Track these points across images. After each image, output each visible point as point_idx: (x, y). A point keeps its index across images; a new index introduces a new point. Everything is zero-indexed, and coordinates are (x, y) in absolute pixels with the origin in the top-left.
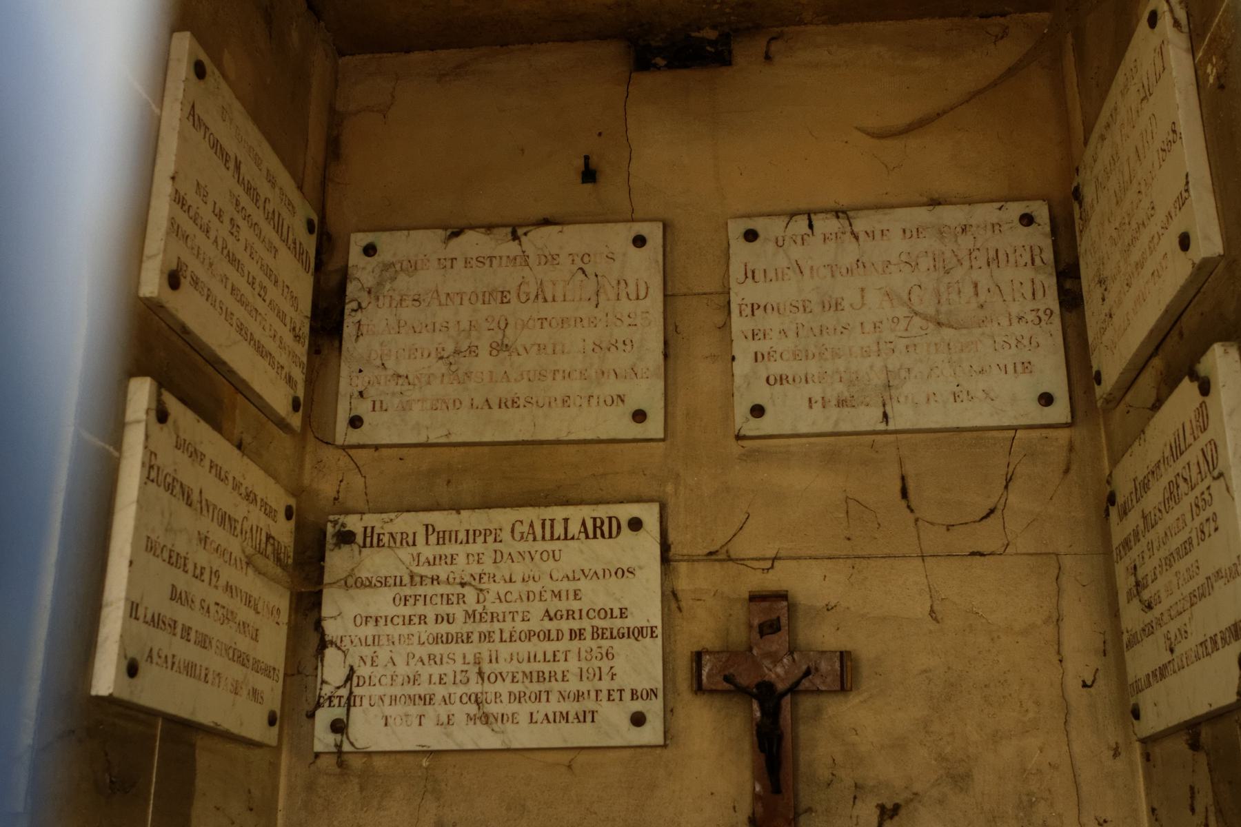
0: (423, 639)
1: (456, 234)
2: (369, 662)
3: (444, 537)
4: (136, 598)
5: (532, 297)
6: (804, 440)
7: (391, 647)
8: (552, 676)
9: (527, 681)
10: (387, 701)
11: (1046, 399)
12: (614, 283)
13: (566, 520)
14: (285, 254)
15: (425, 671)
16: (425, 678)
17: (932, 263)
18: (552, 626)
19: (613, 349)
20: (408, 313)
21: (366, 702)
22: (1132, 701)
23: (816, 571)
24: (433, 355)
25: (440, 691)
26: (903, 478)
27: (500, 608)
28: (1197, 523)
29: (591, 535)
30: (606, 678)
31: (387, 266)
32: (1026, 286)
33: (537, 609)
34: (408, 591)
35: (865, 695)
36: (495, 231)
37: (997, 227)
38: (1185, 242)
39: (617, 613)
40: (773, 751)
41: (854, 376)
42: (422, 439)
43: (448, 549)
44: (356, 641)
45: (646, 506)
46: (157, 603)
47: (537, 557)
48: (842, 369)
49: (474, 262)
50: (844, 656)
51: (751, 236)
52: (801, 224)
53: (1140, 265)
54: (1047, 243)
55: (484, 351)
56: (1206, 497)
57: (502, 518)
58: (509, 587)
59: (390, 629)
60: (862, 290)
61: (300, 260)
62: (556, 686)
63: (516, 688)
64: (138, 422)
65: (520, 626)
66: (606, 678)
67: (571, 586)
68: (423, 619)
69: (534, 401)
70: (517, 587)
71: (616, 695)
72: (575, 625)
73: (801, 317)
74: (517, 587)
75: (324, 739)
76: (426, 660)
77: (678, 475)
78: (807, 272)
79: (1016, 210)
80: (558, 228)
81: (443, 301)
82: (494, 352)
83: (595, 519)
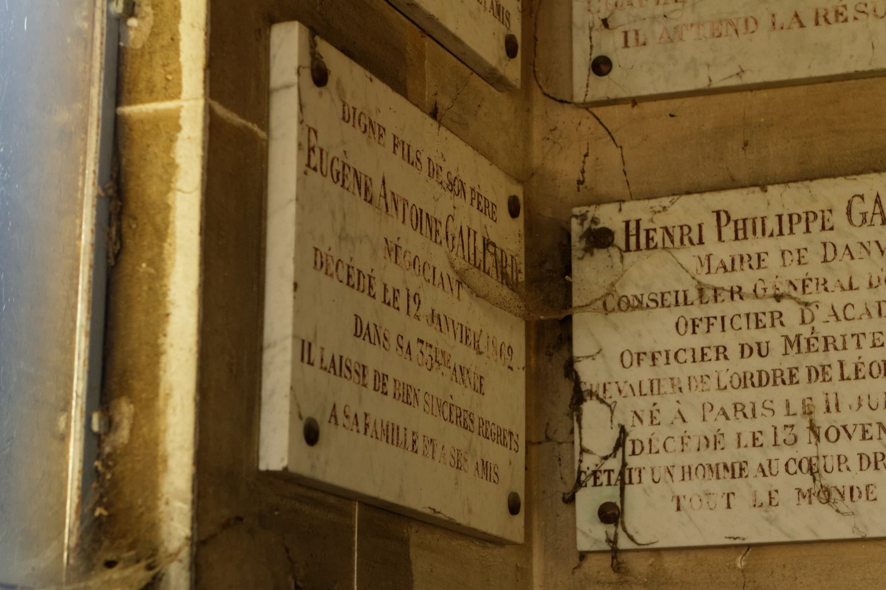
3: (744, 229)
10: (677, 474)
15: (731, 428)
16: (730, 439)
21: (646, 477)
25: (755, 458)
27: (836, 329)
34: (696, 312)
43: (752, 246)
44: (626, 390)
46: (336, 340)
57: (832, 193)
58: (849, 297)
59: (674, 369)
64: (288, 87)
68: (721, 352)
70: (862, 297)
74: (862, 297)
75: (590, 533)
76: (730, 412)
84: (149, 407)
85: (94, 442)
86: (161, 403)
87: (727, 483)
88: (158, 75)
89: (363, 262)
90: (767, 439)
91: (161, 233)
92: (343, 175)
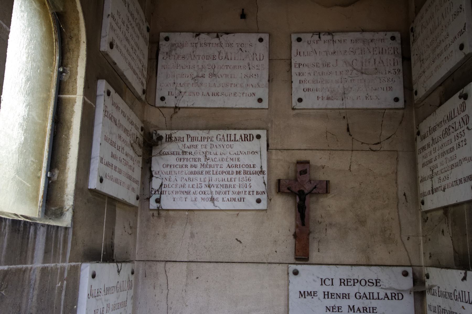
0: (187, 172)
1: (197, 35)
2: (168, 180)
3: (193, 139)
4: (102, 156)
5: (224, 58)
6: (315, 111)
7: (176, 175)
8: (230, 186)
9: (222, 188)
10: (174, 193)
11: (396, 100)
12: (252, 54)
13: (235, 135)
14: (141, 39)
15: (187, 183)
16: (187, 186)
17: (360, 52)
18: (230, 170)
19: (251, 77)
20: (180, 62)
21: (167, 193)
22: (421, 199)
23: (318, 154)
24: (189, 76)
25: (192, 190)
26: (348, 125)
27: (212, 163)
28: (457, 142)
29: (243, 140)
30: (248, 187)
31: (173, 45)
32: (391, 61)
33: (225, 164)
34: (181, 156)
35: (333, 195)
36: (211, 34)
37: (383, 40)
38: (462, 47)
39: (252, 166)
40: (302, 212)
41: (333, 90)
42: (186, 106)
43: (195, 143)
44: (164, 173)
45: (262, 131)
46: (108, 158)
47: (225, 147)
48: (329, 87)
49: (203, 45)
50: (327, 182)
51: (299, 40)
52: (316, 37)
53: (439, 55)
54: (399, 46)
55: (207, 76)
56: (462, 133)
57: (213, 133)
58: (215, 156)
59: (175, 169)
60: (337, 60)
61: (145, 41)
62: (231, 189)
63: (218, 190)
64: (101, 95)
65: (219, 169)
66: (248, 187)
67: (237, 157)
68: (186, 166)
69: (224, 94)
70: (219, 157)
71: (251, 193)
72: (238, 170)
73: (316, 69)
74: (219, 157)
75: (153, 205)
76: (187, 180)
77: (272, 121)
78: (318, 53)
79: (390, 34)
80: (233, 34)
81: (193, 58)
82: (211, 77)
83: (245, 135)
84: (63, 171)
85: (48, 179)
86: (67, 171)
87: (185, 195)
88: (71, 89)
89: (114, 140)
90: (195, 186)
91: (69, 128)
92: (111, 118)
